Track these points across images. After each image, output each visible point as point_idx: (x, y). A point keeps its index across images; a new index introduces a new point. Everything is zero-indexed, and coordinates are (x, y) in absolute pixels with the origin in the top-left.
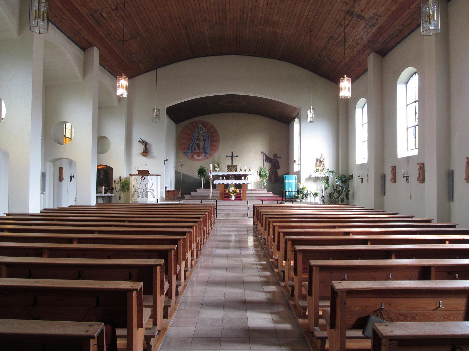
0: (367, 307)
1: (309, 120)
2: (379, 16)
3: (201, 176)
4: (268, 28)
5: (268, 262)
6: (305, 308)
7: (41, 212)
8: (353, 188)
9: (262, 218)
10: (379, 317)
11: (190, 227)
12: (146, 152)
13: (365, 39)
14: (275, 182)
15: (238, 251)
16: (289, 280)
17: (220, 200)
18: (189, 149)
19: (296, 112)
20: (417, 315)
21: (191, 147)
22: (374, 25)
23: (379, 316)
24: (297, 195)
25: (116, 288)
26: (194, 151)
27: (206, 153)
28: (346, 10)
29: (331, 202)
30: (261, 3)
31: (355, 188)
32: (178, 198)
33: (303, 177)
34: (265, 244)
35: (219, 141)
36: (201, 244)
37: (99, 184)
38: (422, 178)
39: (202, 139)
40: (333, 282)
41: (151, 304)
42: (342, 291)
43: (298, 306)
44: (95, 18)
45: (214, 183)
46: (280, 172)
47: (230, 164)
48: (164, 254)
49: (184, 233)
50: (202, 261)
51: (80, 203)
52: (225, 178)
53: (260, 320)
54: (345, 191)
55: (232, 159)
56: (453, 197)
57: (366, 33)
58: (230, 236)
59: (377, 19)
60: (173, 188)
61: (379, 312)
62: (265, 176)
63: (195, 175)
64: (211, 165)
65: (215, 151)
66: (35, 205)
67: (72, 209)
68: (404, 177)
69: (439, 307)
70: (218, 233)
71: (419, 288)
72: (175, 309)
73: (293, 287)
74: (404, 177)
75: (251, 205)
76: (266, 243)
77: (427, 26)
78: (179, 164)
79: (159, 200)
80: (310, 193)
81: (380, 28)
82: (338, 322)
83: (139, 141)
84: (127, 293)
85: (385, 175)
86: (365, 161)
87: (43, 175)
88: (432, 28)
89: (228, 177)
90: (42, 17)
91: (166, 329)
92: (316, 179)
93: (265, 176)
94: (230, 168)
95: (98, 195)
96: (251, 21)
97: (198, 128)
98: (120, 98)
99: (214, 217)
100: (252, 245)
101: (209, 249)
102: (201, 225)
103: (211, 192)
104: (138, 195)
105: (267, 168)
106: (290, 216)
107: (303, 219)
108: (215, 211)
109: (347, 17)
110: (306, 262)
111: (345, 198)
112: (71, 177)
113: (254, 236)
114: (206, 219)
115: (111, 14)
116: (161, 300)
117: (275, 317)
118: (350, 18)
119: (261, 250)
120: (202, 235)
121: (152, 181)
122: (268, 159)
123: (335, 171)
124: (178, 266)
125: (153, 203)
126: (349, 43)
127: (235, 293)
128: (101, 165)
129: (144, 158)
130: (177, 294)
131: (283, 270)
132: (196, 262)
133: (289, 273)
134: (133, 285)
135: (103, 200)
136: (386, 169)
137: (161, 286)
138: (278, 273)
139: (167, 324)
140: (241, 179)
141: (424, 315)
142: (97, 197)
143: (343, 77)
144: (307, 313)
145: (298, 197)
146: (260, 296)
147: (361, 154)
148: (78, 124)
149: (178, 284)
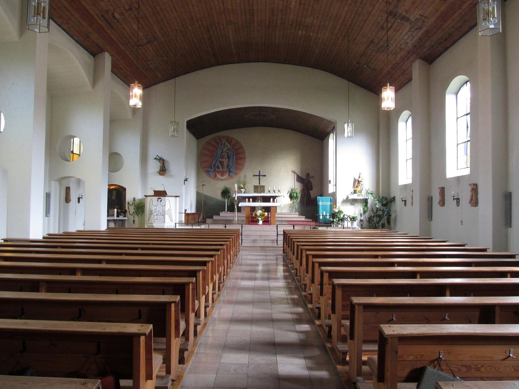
0: (422, 356)
1: (346, 135)
2: (426, 17)
3: (224, 197)
4: (300, 32)
5: (300, 296)
6: (345, 353)
7: (43, 238)
8: (396, 211)
9: (294, 246)
10: (436, 369)
11: (212, 256)
12: (163, 171)
13: (410, 44)
14: (307, 205)
15: (265, 283)
16: (325, 319)
17: (246, 224)
18: (211, 168)
19: (331, 127)
20: (482, 366)
21: (214, 166)
22: (420, 28)
23: (437, 367)
24: (332, 219)
25: (120, 333)
26: (217, 170)
27: (230, 172)
28: (388, 11)
29: (370, 228)
30: (293, 3)
31: (398, 212)
32: (199, 222)
33: (340, 199)
34: (297, 276)
35: (245, 158)
36: (224, 275)
37: (111, 205)
38: (474, 201)
39: (226, 157)
40: (381, 325)
41: (164, 347)
42: (393, 337)
43: (336, 350)
44: (105, 20)
45: (240, 205)
46: (312, 193)
47: (258, 185)
48: (179, 289)
49: (204, 264)
50: (225, 295)
51: (90, 227)
52: (251, 199)
53: (292, 366)
54: (386, 215)
55: (259, 179)
56: (511, 222)
57: (411, 38)
58: (257, 265)
59: (423, 21)
60: (193, 211)
61: (437, 362)
62: (297, 197)
63: (218, 196)
64: (236, 185)
66: (37, 230)
67: (80, 234)
68: (454, 199)
69: (509, 356)
70: (244, 262)
71: (486, 334)
72: (192, 352)
73: (330, 327)
74: (454, 199)
75: (281, 229)
76: (298, 274)
77: (486, 24)
78: (200, 184)
79: (177, 225)
80: (346, 217)
81: (427, 32)
82: (388, 375)
83: (155, 159)
84: (133, 337)
85: (432, 197)
86: (409, 181)
87: (48, 196)
88: (492, 26)
89: (255, 199)
90: (42, 14)
91: (182, 377)
92: (354, 202)
93: (297, 197)
94: (257, 189)
95: (110, 218)
96: (281, 24)
97: (222, 144)
98: (134, 109)
99: (239, 244)
100: (282, 277)
101: (234, 281)
102: (224, 253)
103: (236, 216)
105: (298, 187)
106: (323, 243)
107: (339, 247)
108: (241, 237)
109: (390, 18)
110: (346, 297)
111: (386, 223)
112: (79, 199)
113: (284, 265)
114: (230, 246)
115: (124, 15)
116: (176, 344)
117: (309, 363)
118: (393, 20)
119: (292, 281)
120: (226, 264)
121: (170, 203)
122: (299, 179)
123: (374, 192)
124: (197, 302)
125: (171, 227)
126: (391, 49)
127: (262, 332)
128: (113, 185)
129: (161, 177)
130: (195, 334)
131: (318, 306)
132: (219, 295)
133: (325, 310)
134: (140, 328)
135: (115, 223)
136: (433, 191)
137: (176, 326)
138: (305, 296)
139: (183, 370)
140: (269, 201)
141: (490, 366)
142: (108, 221)
143: (386, 86)
144: (348, 359)
145: (333, 222)
146: (292, 337)
147: (405, 174)
148: (87, 138)
149: (197, 322)
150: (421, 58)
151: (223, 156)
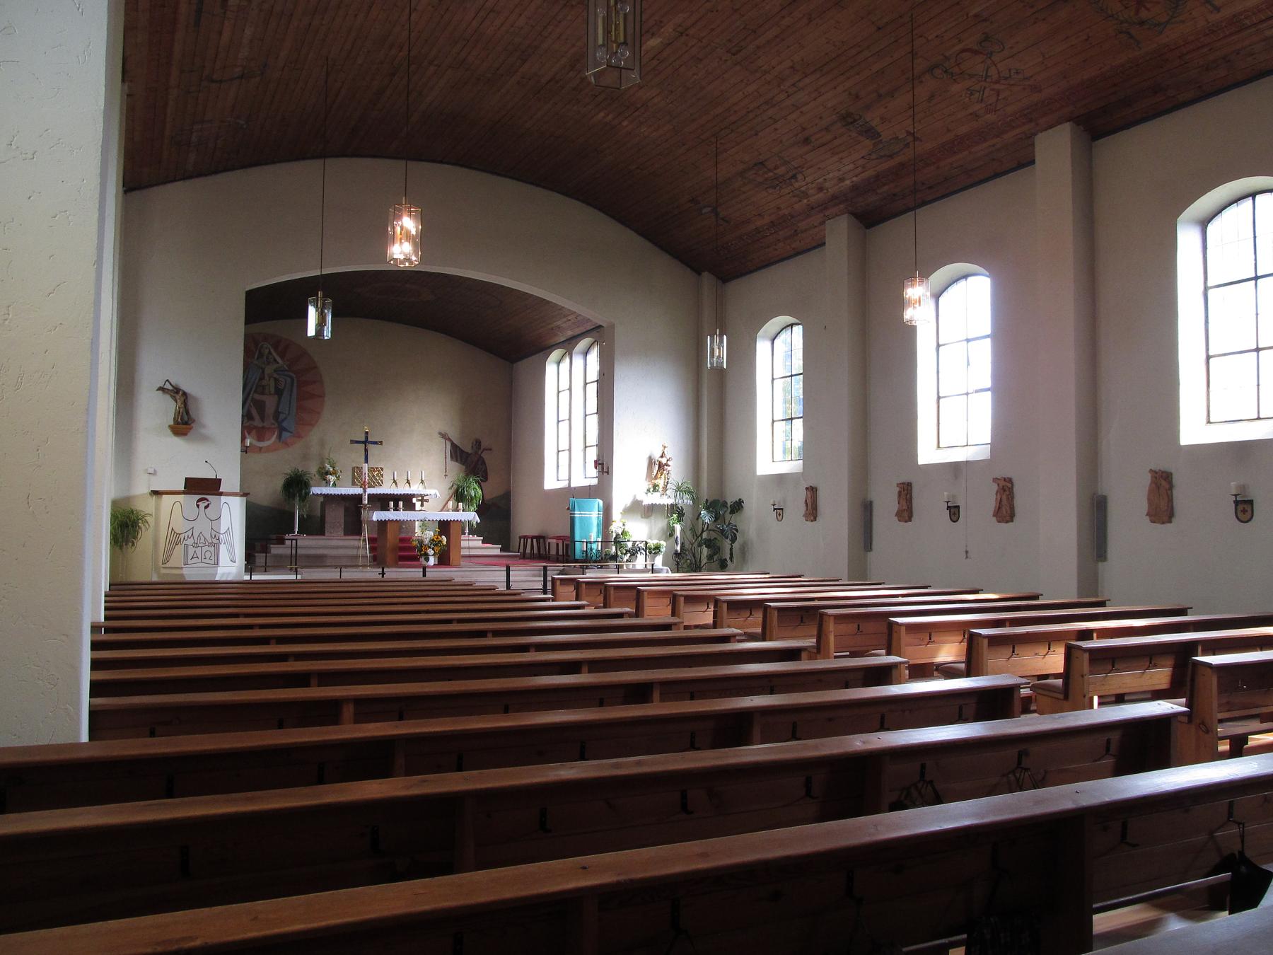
12: (184, 424)
13: (848, 182)
22: (891, 156)
27: (282, 430)
35: (322, 396)
38: (812, 512)
39: (273, 390)
52: (401, 503)
55: (366, 450)
65: (311, 425)
104: (186, 553)
122: (457, 453)
129: (177, 441)
150: (852, 213)
151: (264, 387)
